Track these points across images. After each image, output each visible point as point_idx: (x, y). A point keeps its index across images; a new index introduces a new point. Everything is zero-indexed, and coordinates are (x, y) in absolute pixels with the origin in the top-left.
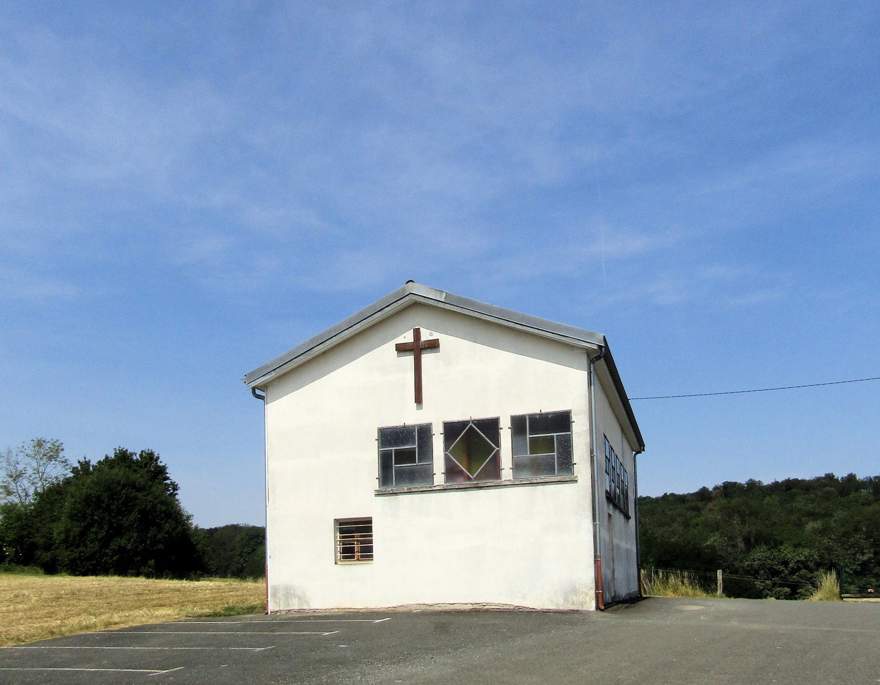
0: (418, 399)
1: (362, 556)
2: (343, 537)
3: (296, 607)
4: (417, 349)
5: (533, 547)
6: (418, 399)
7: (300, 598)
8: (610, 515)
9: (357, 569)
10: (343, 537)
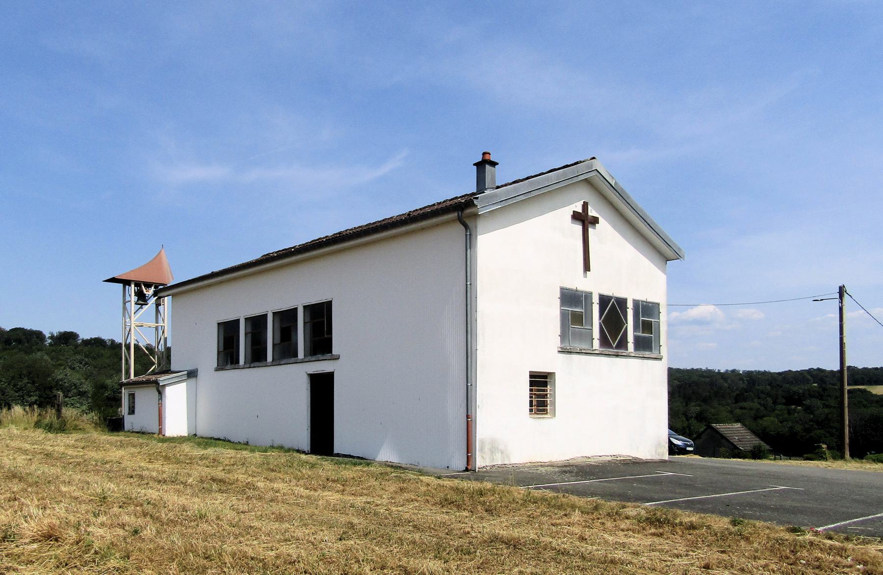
0: (587, 267)
1: (538, 410)
2: (544, 391)
3: (500, 463)
4: (584, 219)
5: (621, 413)
6: (587, 267)
7: (502, 453)
8: (540, 382)
9: (543, 423)
10: (544, 391)
